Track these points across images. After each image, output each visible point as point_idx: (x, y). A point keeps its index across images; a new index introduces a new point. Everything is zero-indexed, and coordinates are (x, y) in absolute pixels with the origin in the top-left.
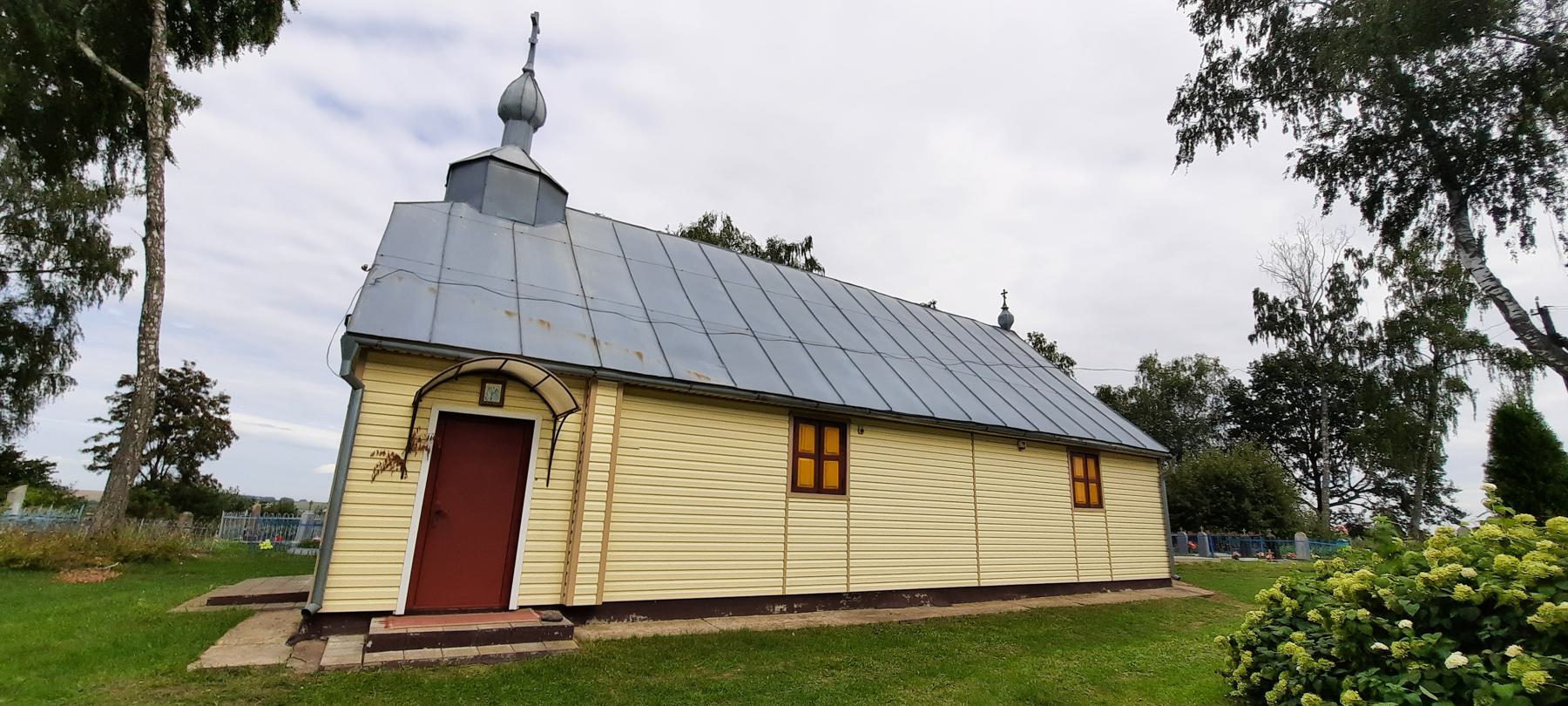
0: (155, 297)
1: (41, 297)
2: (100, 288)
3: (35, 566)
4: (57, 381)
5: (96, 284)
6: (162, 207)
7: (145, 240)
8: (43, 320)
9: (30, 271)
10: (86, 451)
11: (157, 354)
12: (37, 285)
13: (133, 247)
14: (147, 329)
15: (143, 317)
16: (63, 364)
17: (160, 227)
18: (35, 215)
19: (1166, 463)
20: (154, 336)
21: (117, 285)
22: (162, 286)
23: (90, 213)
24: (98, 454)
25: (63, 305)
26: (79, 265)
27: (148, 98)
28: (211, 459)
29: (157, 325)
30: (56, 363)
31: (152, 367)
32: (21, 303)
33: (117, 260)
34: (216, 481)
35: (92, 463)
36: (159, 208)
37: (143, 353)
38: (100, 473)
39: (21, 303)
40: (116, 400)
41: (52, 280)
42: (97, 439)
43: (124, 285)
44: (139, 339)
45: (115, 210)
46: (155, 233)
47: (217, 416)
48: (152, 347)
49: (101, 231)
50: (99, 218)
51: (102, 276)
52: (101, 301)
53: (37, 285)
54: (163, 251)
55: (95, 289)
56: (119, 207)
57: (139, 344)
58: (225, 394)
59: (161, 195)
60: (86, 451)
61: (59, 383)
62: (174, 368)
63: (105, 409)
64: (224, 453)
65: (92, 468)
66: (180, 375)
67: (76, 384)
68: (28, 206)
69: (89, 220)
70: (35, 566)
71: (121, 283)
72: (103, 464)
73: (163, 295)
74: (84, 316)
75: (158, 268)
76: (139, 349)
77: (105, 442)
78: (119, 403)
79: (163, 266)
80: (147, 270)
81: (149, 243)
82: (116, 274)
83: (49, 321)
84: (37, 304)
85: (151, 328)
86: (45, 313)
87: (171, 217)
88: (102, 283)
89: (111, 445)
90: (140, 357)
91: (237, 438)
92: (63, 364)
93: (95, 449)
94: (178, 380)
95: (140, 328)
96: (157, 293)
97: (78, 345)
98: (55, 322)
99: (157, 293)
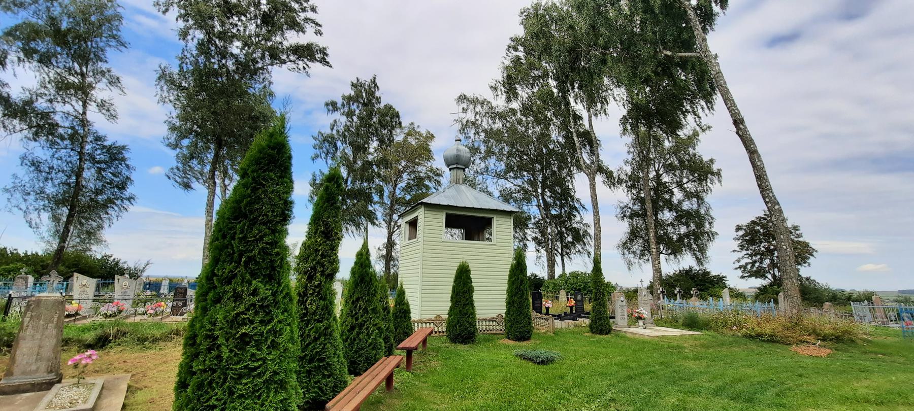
0: (759, 164)
1: (689, 195)
2: (709, 184)
3: (772, 340)
4: (710, 234)
5: (706, 182)
6: (737, 109)
7: (737, 133)
8: (694, 206)
9: (680, 185)
10: (736, 269)
11: (775, 199)
12: (685, 190)
13: (713, 158)
14: (763, 185)
15: (757, 178)
16: (710, 224)
17: (742, 121)
18: (672, 159)
19: (763, 249)
20: (769, 187)
21: (715, 179)
22: (759, 156)
23: (690, 149)
24: (742, 269)
25: (697, 196)
26: (696, 175)
27: (703, 54)
28: (805, 266)
29: (767, 181)
30: (707, 224)
31: (777, 207)
32: (683, 201)
33: (709, 167)
34: (814, 281)
35: (742, 274)
36: (736, 111)
37: (767, 200)
38: (747, 280)
39: (683, 201)
40: (739, 240)
41: (690, 186)
42: (738, 261)
43: (719, 178)
44: (761, 192)
45: (698, 143)
46: (741, 126)
47: (797, 239)
48: (771, 195)
49: (697, 156)
50: (694, 149)
51: (707, 177)
52: (711, 190)
53: (685, 190)
54: (749, 135)
55: (707, 185)
56: (700, 141)
57: (762, 195)
58: (795, 225)
59: (734, 103)
60: (736, 269)
61: (712, 235)
62: (760, 216)
63: (735, 245)
64: (811, 260)
65: (743, 277)
66: (765, 219)
67: (718, 235)
68: (668, 157)
69: (691, 152)
70: (772, 340)
71: (717, 177)
72: (747, 275)
73: (762, 161)
74: (708, 198)
75: (752, 146)
76: (764, 198)
77: (743, 262)
78: (741, 241)
79: (754, 144)
80: (747, 150)
81: (741, 133)
82: (713, 174)
83: (697, 206)
84: (689, 198)
85: (765, 183)
86: (693, 202)
87: (744, 113)
88: (709, 181)
89: (747, 264)
90: (766, 203)
91: (816, 251)
92: (710, 224)
93: (740, 267)
94: (765, 222)
95: (758, 185)
96: (759, 161)
97: (712, 213)
98: (699, 205)
99: (759, 161)
